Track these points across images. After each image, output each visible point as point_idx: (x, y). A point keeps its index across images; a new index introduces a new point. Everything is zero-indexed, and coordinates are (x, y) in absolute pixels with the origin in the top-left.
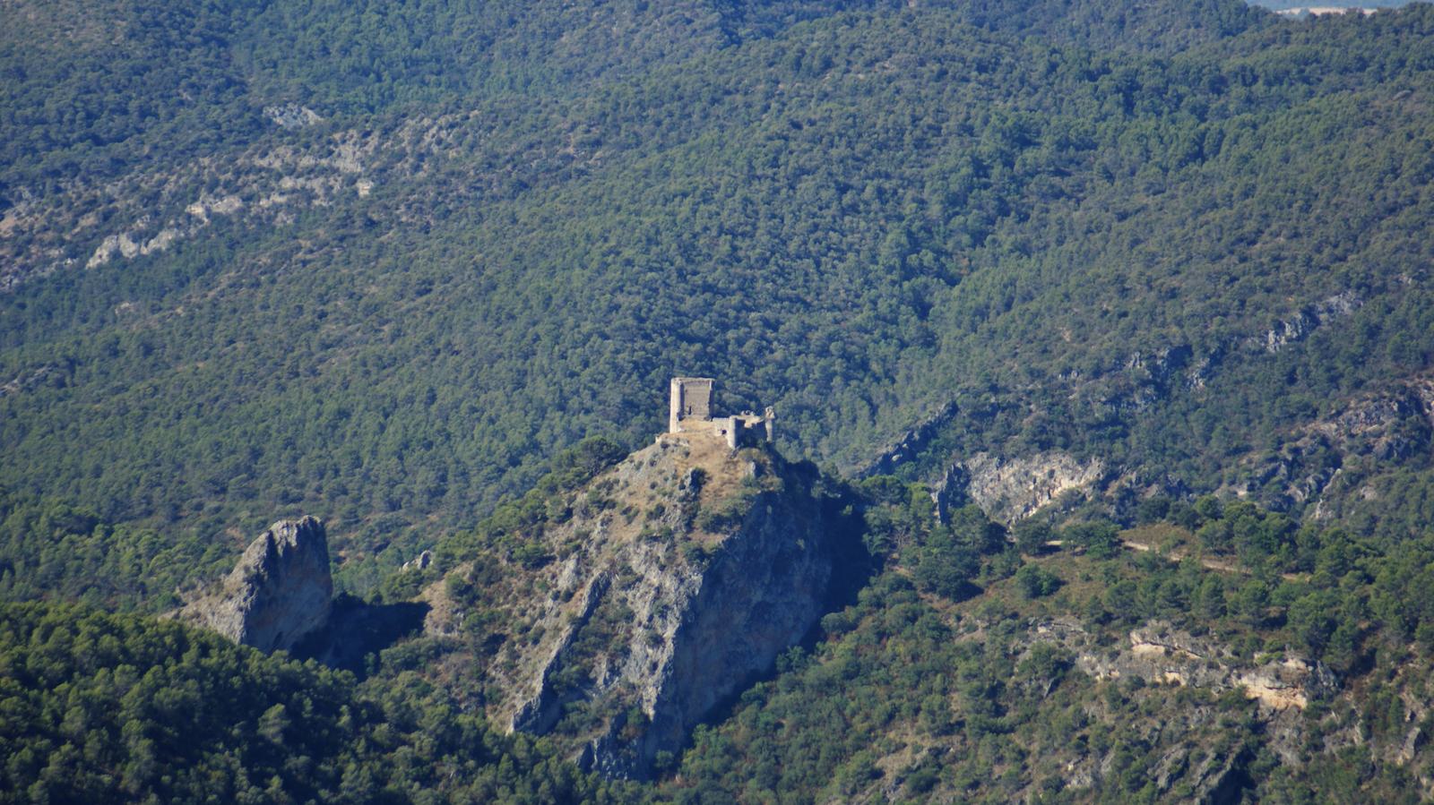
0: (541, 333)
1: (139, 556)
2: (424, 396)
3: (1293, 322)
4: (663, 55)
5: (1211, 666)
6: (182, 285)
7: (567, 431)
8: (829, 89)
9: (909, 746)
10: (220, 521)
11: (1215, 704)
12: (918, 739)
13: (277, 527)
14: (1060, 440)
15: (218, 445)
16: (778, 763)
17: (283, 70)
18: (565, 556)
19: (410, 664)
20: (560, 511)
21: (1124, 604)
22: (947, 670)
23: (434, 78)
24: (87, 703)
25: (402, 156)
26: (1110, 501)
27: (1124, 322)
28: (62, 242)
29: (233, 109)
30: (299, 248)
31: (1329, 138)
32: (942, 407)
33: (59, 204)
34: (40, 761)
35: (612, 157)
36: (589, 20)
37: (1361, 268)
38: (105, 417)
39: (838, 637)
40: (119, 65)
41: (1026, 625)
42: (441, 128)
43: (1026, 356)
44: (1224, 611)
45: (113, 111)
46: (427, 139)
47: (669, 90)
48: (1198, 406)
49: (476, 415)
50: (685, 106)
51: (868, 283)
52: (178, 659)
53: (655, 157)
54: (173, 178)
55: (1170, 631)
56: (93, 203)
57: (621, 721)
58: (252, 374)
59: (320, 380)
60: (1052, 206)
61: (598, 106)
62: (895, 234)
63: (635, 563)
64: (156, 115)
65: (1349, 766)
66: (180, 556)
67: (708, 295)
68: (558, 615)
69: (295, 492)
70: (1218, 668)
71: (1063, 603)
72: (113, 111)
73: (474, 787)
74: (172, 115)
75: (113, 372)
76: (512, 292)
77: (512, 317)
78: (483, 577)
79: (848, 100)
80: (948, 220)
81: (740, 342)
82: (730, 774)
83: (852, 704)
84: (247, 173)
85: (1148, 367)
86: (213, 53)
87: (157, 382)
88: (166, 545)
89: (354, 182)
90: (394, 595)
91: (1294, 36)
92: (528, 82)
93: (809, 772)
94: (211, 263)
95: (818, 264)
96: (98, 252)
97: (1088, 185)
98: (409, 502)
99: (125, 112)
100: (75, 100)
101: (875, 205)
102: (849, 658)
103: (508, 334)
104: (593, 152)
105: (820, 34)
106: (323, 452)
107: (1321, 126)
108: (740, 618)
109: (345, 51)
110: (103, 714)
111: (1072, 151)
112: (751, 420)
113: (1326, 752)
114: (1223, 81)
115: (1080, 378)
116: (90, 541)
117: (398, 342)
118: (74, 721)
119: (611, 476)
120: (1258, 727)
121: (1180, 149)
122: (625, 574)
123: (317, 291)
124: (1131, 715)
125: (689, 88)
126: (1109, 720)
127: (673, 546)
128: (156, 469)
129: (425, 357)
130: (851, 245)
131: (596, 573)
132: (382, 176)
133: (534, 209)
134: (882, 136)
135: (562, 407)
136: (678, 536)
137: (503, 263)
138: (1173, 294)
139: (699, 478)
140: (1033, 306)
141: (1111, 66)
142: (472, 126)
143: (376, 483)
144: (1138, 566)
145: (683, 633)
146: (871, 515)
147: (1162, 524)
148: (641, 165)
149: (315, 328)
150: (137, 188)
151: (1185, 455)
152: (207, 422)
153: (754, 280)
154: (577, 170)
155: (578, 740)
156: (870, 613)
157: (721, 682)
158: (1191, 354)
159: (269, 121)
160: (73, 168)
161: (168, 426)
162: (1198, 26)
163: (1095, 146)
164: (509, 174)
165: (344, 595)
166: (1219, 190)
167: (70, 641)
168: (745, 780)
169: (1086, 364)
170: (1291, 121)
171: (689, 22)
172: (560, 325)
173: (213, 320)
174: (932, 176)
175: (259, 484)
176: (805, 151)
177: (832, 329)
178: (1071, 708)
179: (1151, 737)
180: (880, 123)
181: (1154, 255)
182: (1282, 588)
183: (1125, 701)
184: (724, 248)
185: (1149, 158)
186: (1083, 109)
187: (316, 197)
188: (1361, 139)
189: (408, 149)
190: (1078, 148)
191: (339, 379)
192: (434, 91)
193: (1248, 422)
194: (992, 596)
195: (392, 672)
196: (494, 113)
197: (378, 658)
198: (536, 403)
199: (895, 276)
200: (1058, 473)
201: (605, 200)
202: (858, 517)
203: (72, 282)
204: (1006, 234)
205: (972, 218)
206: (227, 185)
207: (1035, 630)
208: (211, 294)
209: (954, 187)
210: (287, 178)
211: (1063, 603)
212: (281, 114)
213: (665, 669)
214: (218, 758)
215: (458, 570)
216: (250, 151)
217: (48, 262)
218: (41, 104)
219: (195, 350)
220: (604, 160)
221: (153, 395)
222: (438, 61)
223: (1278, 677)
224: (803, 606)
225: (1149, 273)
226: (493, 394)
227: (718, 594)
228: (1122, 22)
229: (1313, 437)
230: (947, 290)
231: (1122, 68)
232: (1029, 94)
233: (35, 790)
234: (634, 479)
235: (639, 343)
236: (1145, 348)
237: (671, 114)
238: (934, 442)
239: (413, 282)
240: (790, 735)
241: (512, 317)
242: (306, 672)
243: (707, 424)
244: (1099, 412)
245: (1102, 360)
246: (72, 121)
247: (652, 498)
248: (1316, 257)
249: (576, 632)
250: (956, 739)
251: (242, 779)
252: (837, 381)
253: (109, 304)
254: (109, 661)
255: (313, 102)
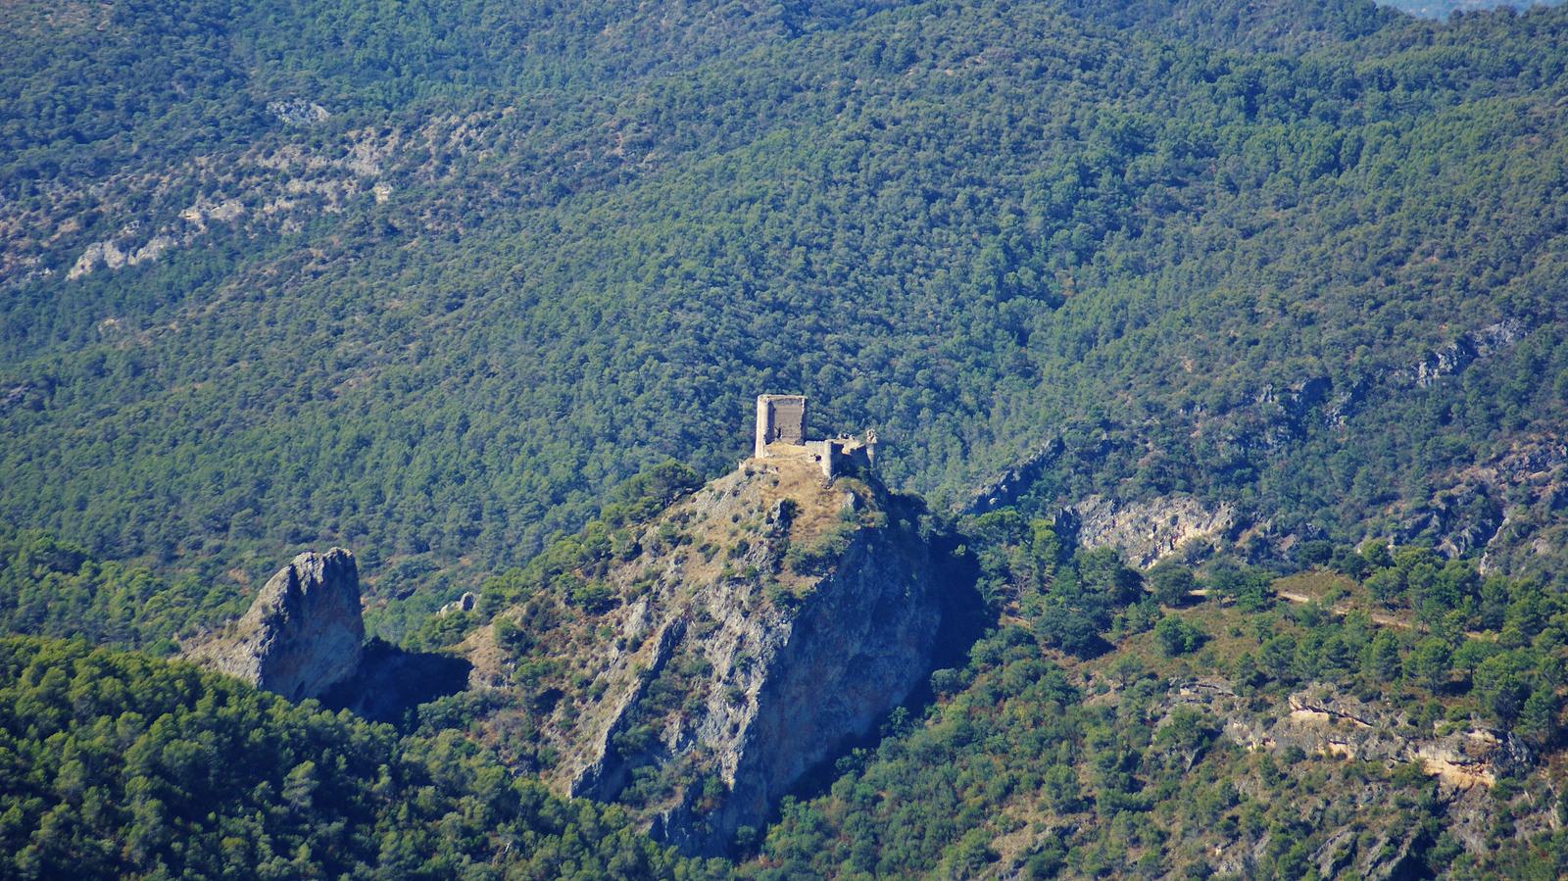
0: (590, 354)
1: (131, 598)
2: (455, 423)
3: (1447, 352)
4: (718, 52)
5: (1383, 737)
6: (175, 299)
7: (619, 464)
8: (913, 86)
9: (1032, 824)
10: (221, 562)
11: (1388, 780)
12: (1040, 816)
13: (298, 560)
14: (1180, 483)
15: (219, 475)
16: (876, 842)
17: (290, 61)
18: (632, 599)
19: (452, 722)
20: (627, 547)
21: (1281, 664)
22: (1074, 737)
23: (459, 73)
24: (85, 757)
25: (425, 157)
26: (1241, 552)
27: (1254, 351)
28: (40, 250)
29: (233, 104)
30: (310, 258)
31: (1486, 146)
32: (1046, 444)
33: (36, 207)
34: (31, 820)
35: (666, 159)
36: (635, 11)
37: (1525, 293)
38: (90, 443)
39: (948, 697)
40: (104, 54)
41: (1167, 686)
42: (470, 127)
43: (1140, 388)
44: (1398, 673)
45: (96, 106)
46: (455, 138)
47: (732, 85)
48: (1337, 447)
49: (515, 445)
50: (750, 103)
51: (960, 305)
52: (192, 708)
53: (718, 159)
54: (166, 179)
55: (1335, 695)
56: (75, 206)
57: (695, 791)
58: (259, 396)
59: (336, 404)
60: (1168, 220)
61: (650, 101)
62: (990, 247)
63: (714, 608)
64: (145, 110)
65: (1545, 855)
66: (179, 598)
67: (779, 314)
68: (624, 666)
69: (306, 529)
70: (1392, 739)
71: (1209, 661)
72: (96, 106)
73: (533, 863)
74: (164, 112)
75: (98, 394)
76: (555, 307)
77: (556, 335)
78: (537, 622)
79: (936, 98)
80: (1050, 234)
81: (815, 369)
82: (821, 854)
83: (964, 775)
84: (250, 175)
85: (1281, 402)
86: (210, 41)
87: (149, 404)
88: (162, 587)
89: (371, 186)
90: (433, 641)
91: (1437, 36)
92: (565, 80)
93: (913, 853)
94: (208, 275)
95: (903, 282)
96: (80, 262)
97: (1209, 198)
98: (437, 542)
99: (110, 107)
100: (54, 92)
101: (968, 216)
102: (961, 721)
103: (552, 355)
104: (644, 154)
105: (902, 24)
106: (340, 486)
107: (1475, 133)
108: (834, 673)
109: (360, 42)
110: (103, 770)
111: (1190, 158)
112: (850, 445)
113: (1518, 838)
114: (1357, 84)
115: (1204, 414)
116: (74, 580)
117: (426, 362)
118: (69, 776)
119: (687, 507)
120: (1438, 808)
121: (1310, 160)
122: (703, 620)
123: (331, 304)
124: (1290, 792)
125: (753, 83)
126: (1263, 798)
127: (759, 589)
128: (149, 502)
129: (457, 380)
130: (940, 261)
131: (669, 619)
132: (402, 179)
133: (580, 216)
134: (976, 138)
135: (613, 439)
136: (764, 578)
137: (546, 273)
138: (1309, 320)
139: (789, 511)
140: (1149, 332)
141: (1231, 65)
142: (505, 126)
143: (399, 521)
144: (1296, 620)
145: (769, 690)
146: (988, 559)
147: (1323, 570)
148: (702, 167)
149: (330, 345)
150: (124, 190)
151: (1323, 503)
152: (208, 449)
153: (830, 296)
154: (625, 174)
155: (647, 811)
156: (985, 671)
157: (812, 747)
158: (1331, 388)
159: (274, 118)
160: (52, 168)
161: (162, 454)
162: (1320, 28)
163: (1215, 154)
164: (549, 177)
165: (376, 639)
166: (1360, 204)
167: (66, 685)
168: (838, 862)
169: (1211, 398)
170: (1440, 127)
171: (748, 14)
172: (610, 344)
173: (212, 336)
174: (1032, 184)
175: (266, 520)
176: (889, 153)
177: (918, 354)
178: (1219, 784)
179: (1313, 818)
180: (973, 123)
181: (1289, 275)
182: (1466, 648)
183: (1283, 777)
184: (798, 261)
185: (1277, 168)
186: (1201, 113)
187: (329, 202)
188: (1522, 148)
189: (433, 151)
190: (1197, 156)
191: (359, 403)
192: (459, 88)
193: (1396, 466)
194: (1126, 654)
195: (430, 730)
196: (531, 110)
197: (415, 713)
198: (582, 433)
199: (990, 296)
200: (1181, 520)
201: (662, 205)
202: (971, 560)
203: (51, 294)
204: (1115, 250)
205: (1078, 232)
206: (226, 187)
207: (1177, 692)
208: (209, 309)
209: (1057, 198)
210: (294, 181)
211: (1209, 661)
212: (288, 110)
213: (747, 732)
214: (239, 824)
215: (508, 614)
216: (253, 150)
217: (22, 272)
218: (16, 95)
219: (190, 372)
220: (657, 163)
221: (144, 419)
222: (464, 54)
223: (1462, 751)
224: (907, 661)
225: (1282, 295)
226: (534, 421)
227: (810, 646)
228: (1235, 22)
229: (1470, 485)
230: (1049, 313)
231: (1244, 68)
232: (1139, 95)
233: (24, 858)
234: (714, 509)
235: (701, 366)
236: (1278, 380)
237: (733, 113)
238: (1036, 483)
239: (443, 294)
240: (891, 810)
241: (556, 335)
242: (339, 727)
243: (801, 449)
244: (1225, 453)
245: (1229, 393)
246: (51, 116)
247: (734, 534)
248: (1474, 280)
249: (645, 687)
250: (1085, 816)
251: (264, 845)
252: (925, 413)
253: (92, 320)
254: (111, 709)
255: (323, 97)
